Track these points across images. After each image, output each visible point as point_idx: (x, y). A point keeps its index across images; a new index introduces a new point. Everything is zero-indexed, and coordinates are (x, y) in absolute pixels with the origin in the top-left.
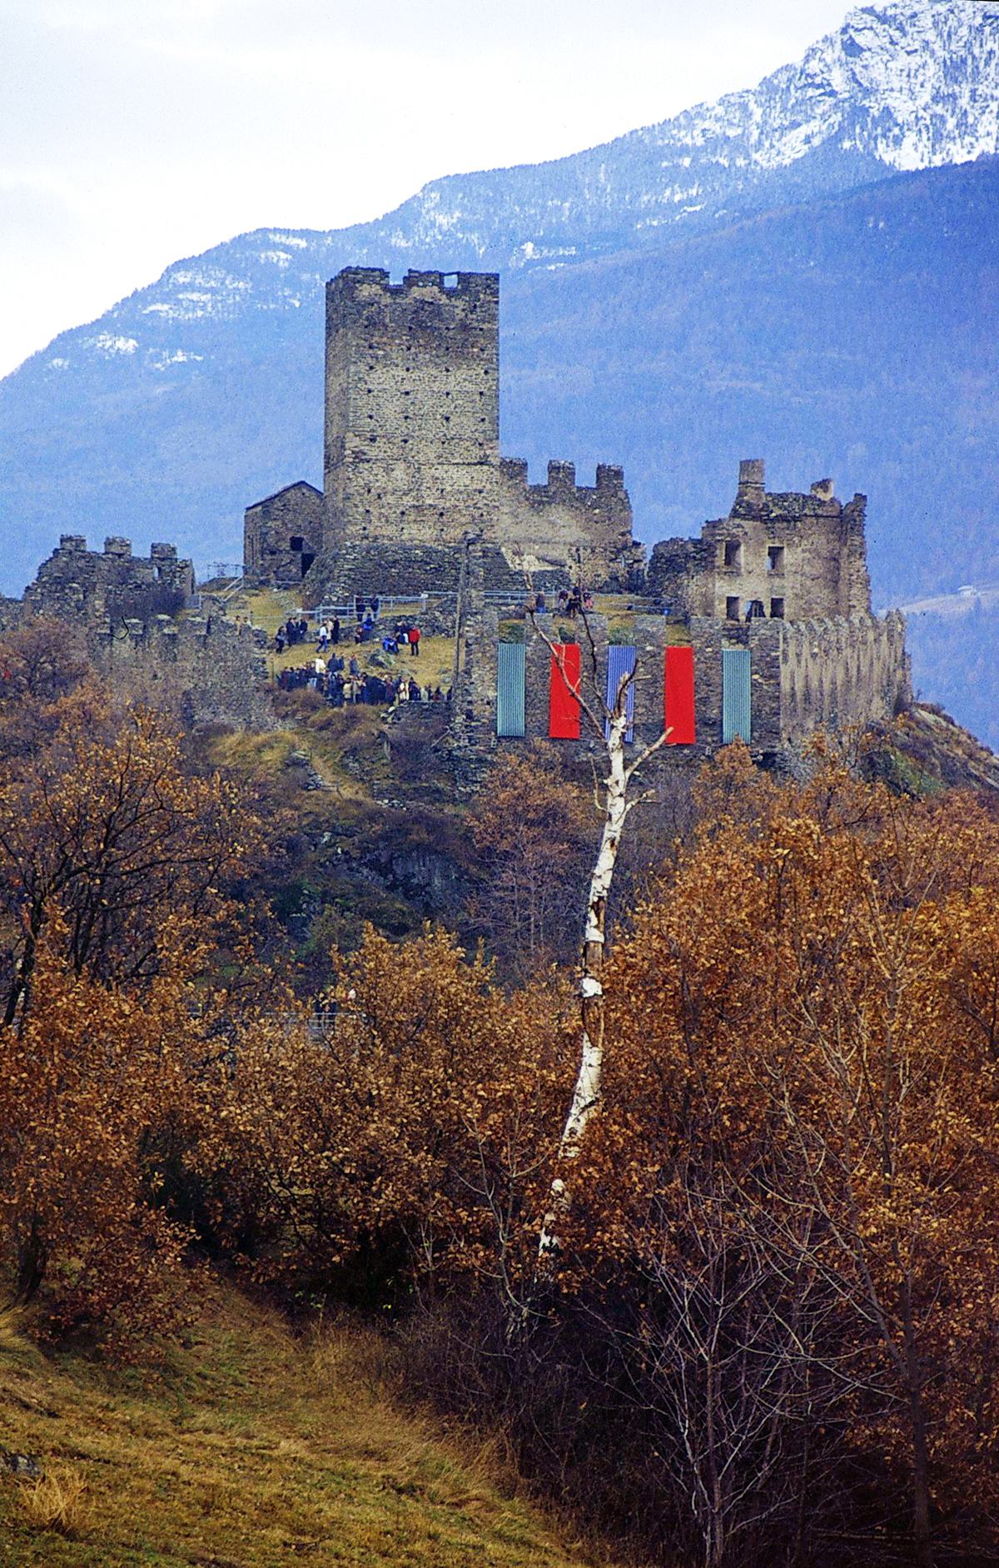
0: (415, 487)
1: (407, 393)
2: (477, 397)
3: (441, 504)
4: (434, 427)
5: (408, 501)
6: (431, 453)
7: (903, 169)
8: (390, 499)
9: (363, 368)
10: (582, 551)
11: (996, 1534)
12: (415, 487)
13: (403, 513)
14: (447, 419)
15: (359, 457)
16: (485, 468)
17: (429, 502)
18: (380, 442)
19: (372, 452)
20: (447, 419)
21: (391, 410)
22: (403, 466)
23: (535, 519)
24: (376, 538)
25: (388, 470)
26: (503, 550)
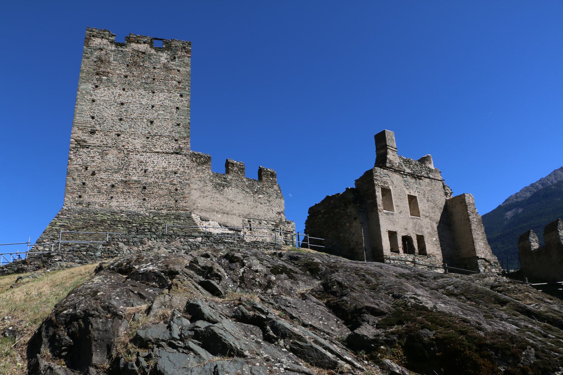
0: (124, 166)
1: (122, 104)
2: (174, 110)
3: (144, 180)
4: (142, 128)
5: (118, 177)
6: (138, 143)
7: (439, 219)
8: (103, 175)
9: (90, 86)
10: (252, 222)
11: (560, 286)
12: (124, 166)
13: (113, 186)
14: (152, 122)
15: (81, 144)
16: (179, 156)
17: (135, 178)
18: (98, 135)
19: (92, 140)
20: (152, 122)
21: (110, 113)
22: (116, 152)
23: (218, 195)
24: (89, 204)
25: (103, 154)
26: (193, 215)
